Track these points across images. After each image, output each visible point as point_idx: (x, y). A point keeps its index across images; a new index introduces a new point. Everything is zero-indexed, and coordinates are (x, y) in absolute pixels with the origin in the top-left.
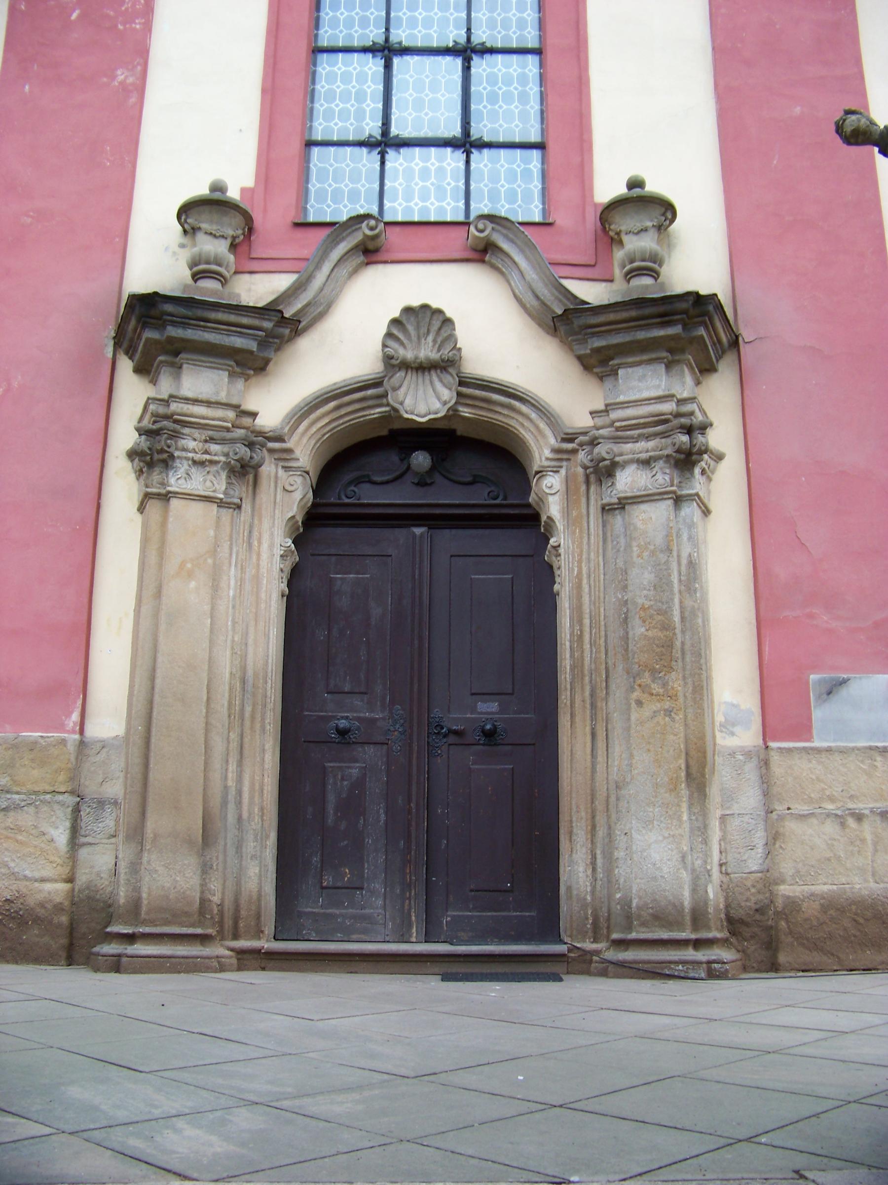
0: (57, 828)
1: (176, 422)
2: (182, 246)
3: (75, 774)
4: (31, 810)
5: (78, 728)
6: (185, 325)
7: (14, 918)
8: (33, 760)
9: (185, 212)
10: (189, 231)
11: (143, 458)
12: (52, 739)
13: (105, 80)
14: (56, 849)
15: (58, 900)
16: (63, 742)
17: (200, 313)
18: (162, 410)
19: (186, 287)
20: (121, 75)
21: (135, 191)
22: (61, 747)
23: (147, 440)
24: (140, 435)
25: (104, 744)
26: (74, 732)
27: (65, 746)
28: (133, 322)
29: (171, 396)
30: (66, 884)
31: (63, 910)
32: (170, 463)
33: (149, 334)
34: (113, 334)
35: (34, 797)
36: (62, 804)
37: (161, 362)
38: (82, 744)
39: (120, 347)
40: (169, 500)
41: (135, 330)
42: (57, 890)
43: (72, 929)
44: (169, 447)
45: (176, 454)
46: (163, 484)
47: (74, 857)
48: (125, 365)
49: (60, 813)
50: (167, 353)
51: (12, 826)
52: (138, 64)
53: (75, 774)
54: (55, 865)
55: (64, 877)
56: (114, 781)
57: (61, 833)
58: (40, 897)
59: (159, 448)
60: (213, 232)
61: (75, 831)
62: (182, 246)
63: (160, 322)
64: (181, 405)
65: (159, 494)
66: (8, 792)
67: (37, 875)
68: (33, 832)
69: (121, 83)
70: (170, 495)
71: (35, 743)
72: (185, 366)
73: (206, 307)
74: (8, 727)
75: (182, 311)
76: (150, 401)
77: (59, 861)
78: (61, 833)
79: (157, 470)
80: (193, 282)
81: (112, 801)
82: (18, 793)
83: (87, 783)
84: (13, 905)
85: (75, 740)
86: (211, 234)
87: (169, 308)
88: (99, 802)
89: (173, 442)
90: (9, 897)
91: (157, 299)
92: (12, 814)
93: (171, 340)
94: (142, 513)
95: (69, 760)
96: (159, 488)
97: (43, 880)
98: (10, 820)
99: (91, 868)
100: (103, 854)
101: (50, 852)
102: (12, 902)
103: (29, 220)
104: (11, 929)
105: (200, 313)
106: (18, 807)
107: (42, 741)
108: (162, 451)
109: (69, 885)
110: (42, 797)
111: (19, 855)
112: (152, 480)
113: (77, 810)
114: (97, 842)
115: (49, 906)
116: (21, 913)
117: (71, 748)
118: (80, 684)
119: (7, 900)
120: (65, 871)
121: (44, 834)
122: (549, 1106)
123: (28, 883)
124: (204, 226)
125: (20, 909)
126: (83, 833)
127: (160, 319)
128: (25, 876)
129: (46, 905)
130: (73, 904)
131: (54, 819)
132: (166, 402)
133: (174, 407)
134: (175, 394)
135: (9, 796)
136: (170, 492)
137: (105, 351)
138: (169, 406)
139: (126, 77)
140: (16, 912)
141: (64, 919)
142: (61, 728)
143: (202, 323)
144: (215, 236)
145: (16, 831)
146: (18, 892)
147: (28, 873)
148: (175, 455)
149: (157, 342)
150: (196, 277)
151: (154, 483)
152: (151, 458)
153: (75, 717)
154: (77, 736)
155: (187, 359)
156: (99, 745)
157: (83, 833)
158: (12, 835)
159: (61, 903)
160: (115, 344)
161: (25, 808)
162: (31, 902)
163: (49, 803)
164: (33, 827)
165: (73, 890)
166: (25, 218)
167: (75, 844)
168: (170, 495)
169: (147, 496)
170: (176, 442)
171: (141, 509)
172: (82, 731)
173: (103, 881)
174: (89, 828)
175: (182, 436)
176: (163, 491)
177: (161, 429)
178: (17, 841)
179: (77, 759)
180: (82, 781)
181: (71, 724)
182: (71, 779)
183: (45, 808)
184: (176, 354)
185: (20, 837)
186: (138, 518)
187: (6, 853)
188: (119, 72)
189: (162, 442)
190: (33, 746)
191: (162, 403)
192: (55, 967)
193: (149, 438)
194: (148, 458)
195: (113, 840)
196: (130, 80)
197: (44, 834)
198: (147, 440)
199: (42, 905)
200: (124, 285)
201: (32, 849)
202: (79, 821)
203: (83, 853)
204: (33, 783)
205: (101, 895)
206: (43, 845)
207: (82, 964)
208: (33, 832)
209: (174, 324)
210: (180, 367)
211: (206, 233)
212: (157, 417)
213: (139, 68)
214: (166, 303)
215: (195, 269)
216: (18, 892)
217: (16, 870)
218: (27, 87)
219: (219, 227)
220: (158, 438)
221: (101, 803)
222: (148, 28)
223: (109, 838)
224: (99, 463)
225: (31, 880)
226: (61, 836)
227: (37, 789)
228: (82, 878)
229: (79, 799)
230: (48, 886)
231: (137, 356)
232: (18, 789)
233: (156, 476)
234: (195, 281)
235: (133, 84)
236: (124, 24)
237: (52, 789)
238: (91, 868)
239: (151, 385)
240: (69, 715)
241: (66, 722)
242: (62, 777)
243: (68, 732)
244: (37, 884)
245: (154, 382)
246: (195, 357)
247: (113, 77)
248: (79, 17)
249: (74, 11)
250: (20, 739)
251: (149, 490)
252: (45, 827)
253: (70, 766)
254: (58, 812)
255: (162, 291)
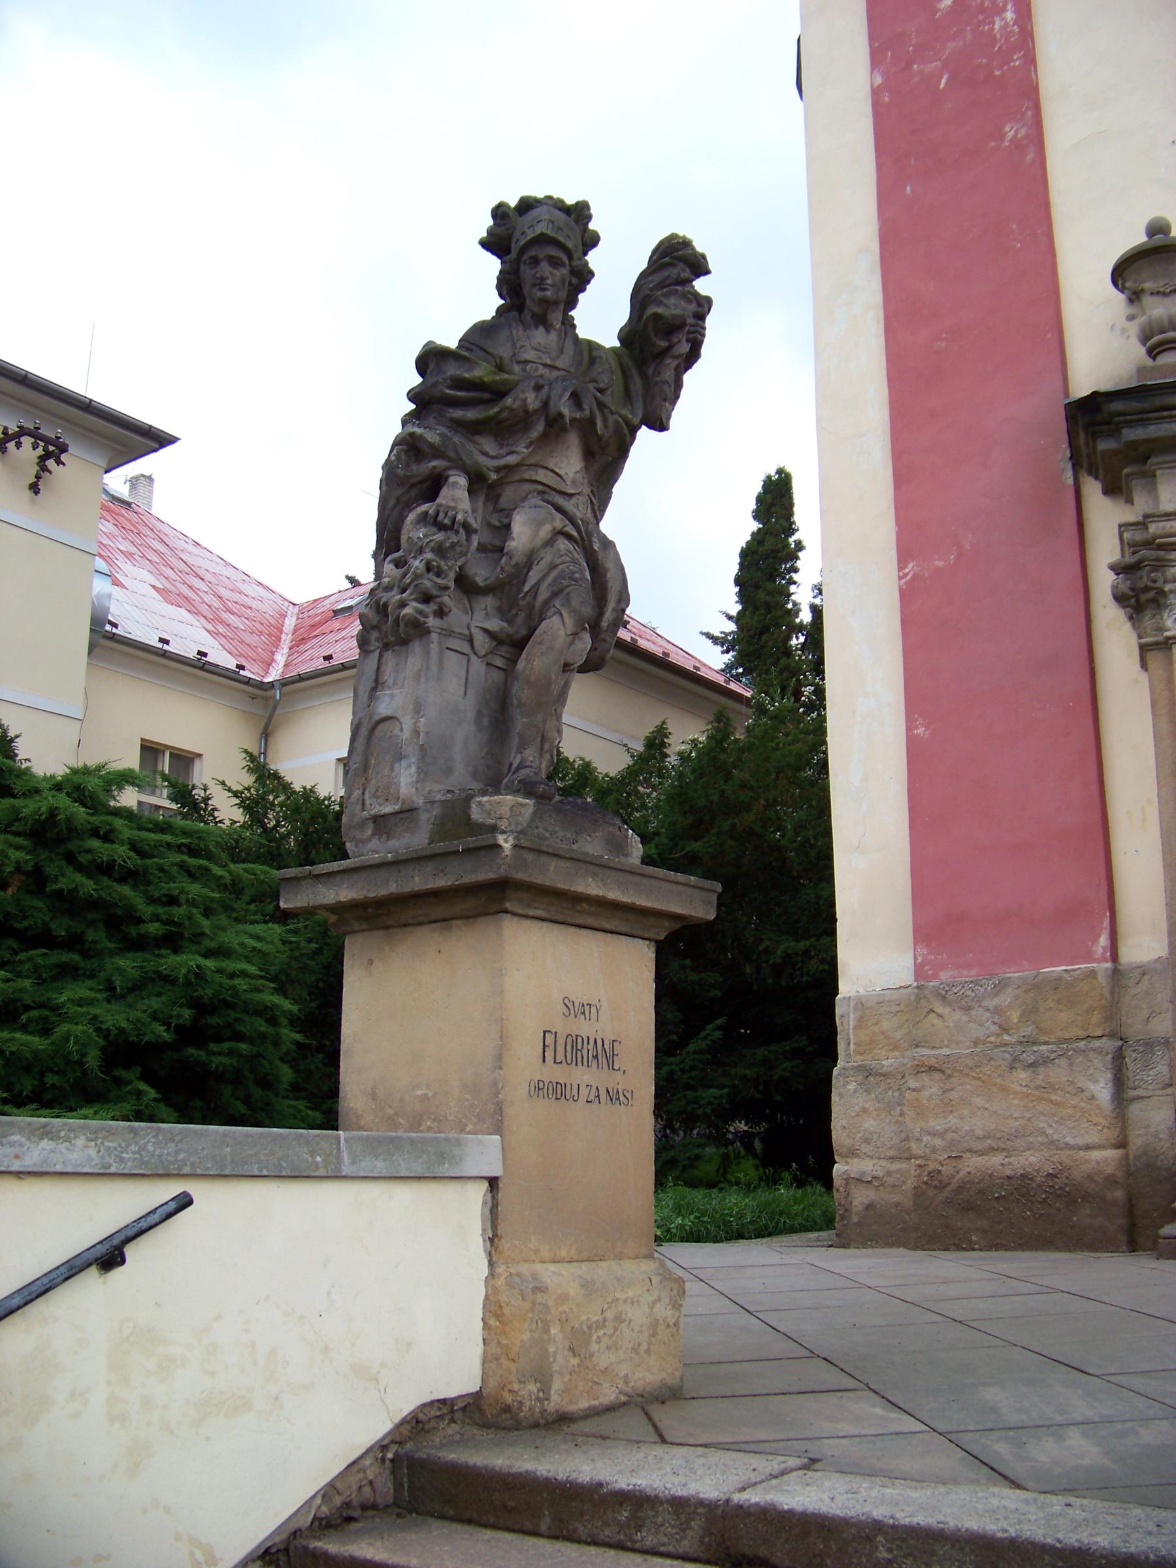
0: (1097, 1081)
1: (1161, 547)
2: (1131, 318)
3: (1112, 1012)
4: (1063, 1062)
5: (1109, 954)
6: (1143, 422)
7: (1059, 1196)
8: (1059, 1001)
9: (1121, 275)
10: (1135, 297)
11: (1127, 603)
12: (1079, 972)
13: (993, 144)
14: (1099, 1108)
15: (1109, 1170)
16: (1092, 974)
17: (1158, 401)
18: (1139, 536)
19: (1141, 370)
20: (1010, 132)
21: (1059, 268)
22: (1090, 980)
23: (1126, 579)
24: (1117, 574)
25: (1143, 970)
26: (1104, 960)
27: (1095, 977)
28: (1082, 436)
29: (1146, 516)
30: (1117, 1151)
31: (1117, 1183)
32: (1162, 601)
33: (1104, 445)
34: (1068, 454)
35: (1064, 1046)
36: (1099, 1051)
37: (1128, 475)
38: (1117, 973)
39: (1082, 467)
40: (1171, 648)
41: (1087, 444)
42: (1106, 1158)
43: (1130, 1206)
44: (1155, 581)
45: (1167, 588)
46: (1160, 629)
47: (1124, 1115)
48: (1092, 489)
49: (1097, 1062)
50: (1134, 461)
51: (1043, 1084)
52: (1027, 109)
53: (1112, 1012)
54: (1100, 1128)
55: (1113, 1141)
56: (1163, 1015)
57: (1103, 1088)
58: (1087, 1168)
59: (1142, 586)
60: (1162, 289)
61: (1119, 1083)
62: (1131, 318)
63: (1113, 427)
64: (1161, 524)
65: (1157, 644)
66: (1034, 1043)
67: (1081, 1141)
68: (1069, 1089)
69: (1012, 140)
70: (1171, 641)
71: (1060, 979)
72: (1158, 472)
73: (1165, 391)
74: (1026, 964)
75: (1135, 405)
76: (1123, 529)
77: (1104, 1122)
78: (1103, 1088)
79: (1148, 613)
80: (1151, 360)
81: (1163, 1041)
82: (1046, 1043)
83: (1129, 1021)
84: (1056, 1180)
85: (1106, 969)
86: (1158, 293)
87: (1117, 406)
88: (1147, 1044)
89: (1159, 575)
90: (1051, 1171)
91: (1099, 399)
92: (1041, 1069)
93: (1133, 445)
94: (1146, 670)
95: (1102, 995)
96: (1155, 636)
97: (1088, 1147)
98: (1040, 1077)
99: (1145, 1128)
100: (1159, 1108)
101: (1092, 1113)
102: (1056, 1177)
103: (943, 344)
104: (1058, 1210)
105: (1158, 401)
106: (1047, 1061)
107: (1066, 976)
108: (1147, 589)
109: (1120, 1152)
110: (1074, 1045)
111: (1056, 1119)
112: (1145, 628)
113: (1119, 1059)
114: (1151, 1093)
115: (1099, 1179)
116: (1067, 1189)
117: (1102, 979)
118: (1104, 898)
119: (1049, 1175)
120: (1113, 1134)
121: (1083, 1091)
122: (808, 1354)
123: (1071, 1152)
124: (1147, 285)
125: (1066, 1185)
126: (1131, 1084)
127: (1109, 423)
128: (1066, 1144)
129: (1096, 1178)
130: (1129, 1174)
131: (1092, 1071)
132: (1142, 525)
133: (1153, 528)
134: (1149, 511)
135: (1035, 1048)
136: (1169, 638)
137: (1064, 478)
138: (1147, 528)
139: (1017, 131)
140: (1060, 1188)
141: (1119, 1194)
142: (1088, 957)
143: (1165, 413)
144: (1165, 294)
145: (1049, 1090)
146: (1061, 1164)
147: (1069, 1140)
148: (1166, 589)
149: (1116, 452)
150: (1153, 352)
151: (1148, 631)
152: (1137, 601)
153: (1104, 940)
154: (1109, 965)
155: (1160, 463)
156: (1137, 972)
157: (1131, 1084)
158: (1045, 1095)
159: (1113, 1175)
160: (1074, 466)
161: (1057, 1060)
162: (1077, 1174)
163: (1084, 1051)
164: (1068, 1083)
165: (1127, 1156)
166: (938, 343)
167: (1123, 1099)
168: (1171, 641)
169: (1144, 649)
170: (1163, 573)
171: (1144, 665)
172: (1115, 957)
173: (1162, 1143)
174: (1137, 1077)
175: (1169, 564)
176: (1160, 639)
177: (1140, 561)
178: (1052, 1102)
179: (1112, 993)
180: (1124, 1019)
181: (1100, 950)
182: (1108, 1019)
183: (1080, 1059)
184: (1144, 459)
185: (1054, 1097)
186: (1143, 678)
187: (1041, 1118)
188: (1007, 128)
189: (1144, 578)
190: (1056, 983)
191: (1139, 527)
192: (1113, 1254)
193: (1129, 576)
194: (1133, 601)
195: (1169, 1091)
196: (1022, 133)
197: (1083, 1091)
198: (1126, 579)
199: (1090, 1178)
200: (1070, 389)
201: (1070, 1111)
202: (1124, 1070)
203: (1134, 1110)
204: (1062, 1029)
205: (1162, 1161)
206: (1083, 1104)
207: (1150, 1250)
208: (1069, 1089)
209: (1129, 424)
210: (1154, 476)
211: (1152, 294)
212: (1135, 546)
213: (1029, 113)
214: (1112, 401)
215: (1148, 344)
216: (1061, 1164)
217: (1055, 1137)
218: (908, 188)
219: (1166, 281)
220: (1139, 573)
221: (1149, 1045)
222: (1030, 60)
223: (1164, 1089)
224: (1082, 619)
225: (1075, 1149)
226: (1102, 1091)
227: (1068, 1036)
228: (1137, 1142)
229: (1121, 1043)
230: (1096, 1155)
231: (1101, 476)
232: (1043, 1038)
233: (1148, 622)
234: (1154, 358)
235: (1026, 136)
236: (1000, 67)
237: (1085, 1034)
238: (1145, 1128)
239: (1129, 505)
240: (1096, 939)
241: (1094, 949)
242: (1095, 1018)
243: (1098, 961)
244: (1082, 1153)
245: (1129, 501)
246: (1168, 458)
247: (1002, 137)
248: (947, 84)
249: (941, 78)
250: (1040, 977)
251: (1143, 641)
252: (1082, 1082)
253: (1103, 1002)
254: (1096, 1061)
255: (1105, 386)
